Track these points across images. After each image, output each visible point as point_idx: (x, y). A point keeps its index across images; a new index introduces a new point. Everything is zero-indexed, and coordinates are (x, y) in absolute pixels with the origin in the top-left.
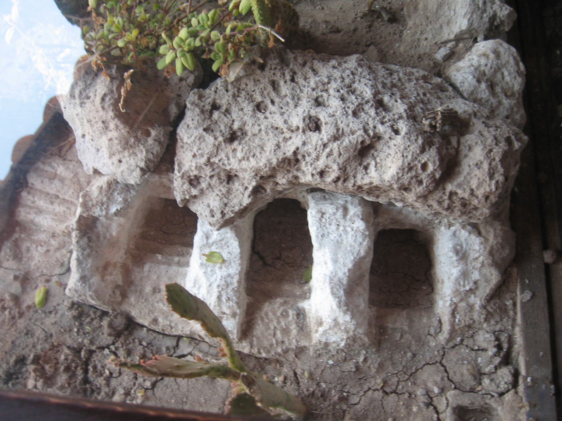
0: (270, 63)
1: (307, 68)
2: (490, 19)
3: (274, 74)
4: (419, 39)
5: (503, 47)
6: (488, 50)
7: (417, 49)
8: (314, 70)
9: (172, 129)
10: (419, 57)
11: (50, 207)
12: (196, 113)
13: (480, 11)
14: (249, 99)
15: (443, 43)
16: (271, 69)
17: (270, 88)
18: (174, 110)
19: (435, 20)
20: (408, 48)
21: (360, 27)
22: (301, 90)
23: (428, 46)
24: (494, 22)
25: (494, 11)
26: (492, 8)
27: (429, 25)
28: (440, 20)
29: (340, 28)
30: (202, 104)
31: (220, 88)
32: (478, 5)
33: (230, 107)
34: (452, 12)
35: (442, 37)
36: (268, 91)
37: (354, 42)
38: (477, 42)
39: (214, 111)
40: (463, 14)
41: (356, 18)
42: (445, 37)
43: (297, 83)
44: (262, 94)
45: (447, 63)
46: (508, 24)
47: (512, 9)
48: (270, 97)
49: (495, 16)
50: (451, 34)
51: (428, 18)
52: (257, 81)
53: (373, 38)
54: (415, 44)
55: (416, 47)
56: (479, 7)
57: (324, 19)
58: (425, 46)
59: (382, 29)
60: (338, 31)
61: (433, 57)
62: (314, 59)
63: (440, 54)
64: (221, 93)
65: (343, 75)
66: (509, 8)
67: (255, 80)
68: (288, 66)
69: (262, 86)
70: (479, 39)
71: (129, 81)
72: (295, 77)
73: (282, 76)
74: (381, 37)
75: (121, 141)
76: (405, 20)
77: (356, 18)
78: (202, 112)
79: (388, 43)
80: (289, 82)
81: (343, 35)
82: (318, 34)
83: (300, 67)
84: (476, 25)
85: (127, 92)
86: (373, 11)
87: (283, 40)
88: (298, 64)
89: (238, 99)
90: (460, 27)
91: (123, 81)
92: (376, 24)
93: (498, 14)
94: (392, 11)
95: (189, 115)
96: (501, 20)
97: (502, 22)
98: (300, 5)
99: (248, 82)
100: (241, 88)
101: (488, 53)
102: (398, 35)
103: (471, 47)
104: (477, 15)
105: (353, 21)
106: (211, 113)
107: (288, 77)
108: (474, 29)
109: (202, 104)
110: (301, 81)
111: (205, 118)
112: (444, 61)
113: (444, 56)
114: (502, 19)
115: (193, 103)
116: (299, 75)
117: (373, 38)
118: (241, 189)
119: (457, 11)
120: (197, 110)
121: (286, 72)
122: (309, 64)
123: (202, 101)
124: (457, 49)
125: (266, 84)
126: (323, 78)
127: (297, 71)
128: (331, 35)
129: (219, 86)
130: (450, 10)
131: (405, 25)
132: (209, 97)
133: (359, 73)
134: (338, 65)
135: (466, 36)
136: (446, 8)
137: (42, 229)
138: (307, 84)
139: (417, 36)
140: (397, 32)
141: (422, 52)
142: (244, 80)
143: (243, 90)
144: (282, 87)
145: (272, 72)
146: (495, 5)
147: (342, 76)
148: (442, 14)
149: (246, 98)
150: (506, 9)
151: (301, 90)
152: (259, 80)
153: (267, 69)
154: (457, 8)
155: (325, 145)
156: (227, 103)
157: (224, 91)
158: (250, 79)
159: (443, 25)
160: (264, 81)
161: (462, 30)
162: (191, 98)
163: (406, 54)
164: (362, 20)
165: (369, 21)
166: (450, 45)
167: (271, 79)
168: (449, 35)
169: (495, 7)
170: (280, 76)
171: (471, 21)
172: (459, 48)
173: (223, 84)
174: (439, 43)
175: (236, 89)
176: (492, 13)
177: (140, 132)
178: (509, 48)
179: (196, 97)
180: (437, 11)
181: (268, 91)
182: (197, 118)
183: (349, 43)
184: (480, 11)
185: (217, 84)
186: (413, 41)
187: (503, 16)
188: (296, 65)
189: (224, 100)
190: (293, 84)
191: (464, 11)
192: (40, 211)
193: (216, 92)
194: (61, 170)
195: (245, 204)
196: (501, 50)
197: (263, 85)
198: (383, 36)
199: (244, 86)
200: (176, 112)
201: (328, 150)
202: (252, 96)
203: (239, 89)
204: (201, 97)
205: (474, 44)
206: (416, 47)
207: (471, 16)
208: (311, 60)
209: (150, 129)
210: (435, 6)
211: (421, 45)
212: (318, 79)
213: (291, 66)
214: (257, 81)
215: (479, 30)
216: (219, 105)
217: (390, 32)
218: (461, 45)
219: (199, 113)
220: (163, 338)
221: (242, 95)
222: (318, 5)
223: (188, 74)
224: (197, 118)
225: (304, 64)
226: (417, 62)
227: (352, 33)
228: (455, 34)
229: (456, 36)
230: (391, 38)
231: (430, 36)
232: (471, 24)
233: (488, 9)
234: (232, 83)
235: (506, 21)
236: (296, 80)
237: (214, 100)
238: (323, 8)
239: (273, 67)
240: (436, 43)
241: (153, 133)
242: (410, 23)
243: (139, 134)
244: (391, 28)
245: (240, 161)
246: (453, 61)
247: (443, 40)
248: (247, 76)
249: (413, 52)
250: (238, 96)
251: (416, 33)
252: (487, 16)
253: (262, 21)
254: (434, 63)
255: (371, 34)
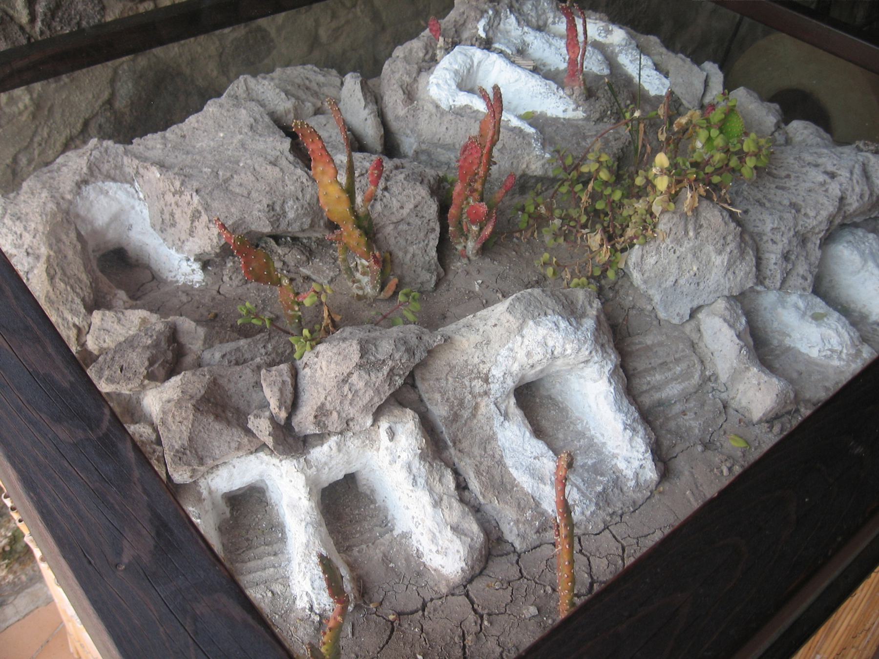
11: (669, 375)
75: (634, 430)
118: (813, 246)
137: (673, 402)
155: (851, 179)
192: (658, 388)
194: (649, 340)
195: (819, 257)
201: (855, 181)
220: (495, 163)
245: (815, 217)
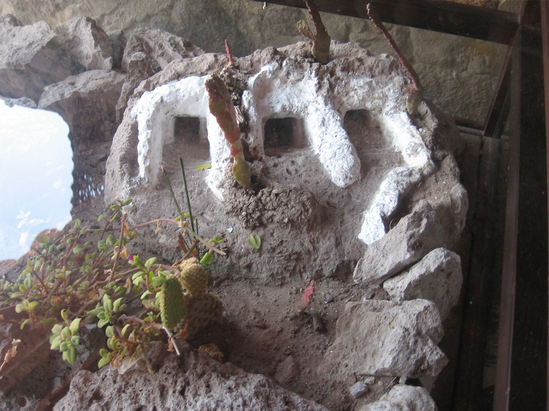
0: (167, 365)
1: (202, 382)
2: (417, 361)
3: (166, 379)
4: (339, 364)
5: (422, 400)
6: (404, 401)
7: (334, 375)
8: (208, 386)
9: (49, 403)
10: (333, 386)
12: (74, 399)
14: (132, 399)
15: (362, 375)
16: (165, 372)
17: (157, 393)
18: (58, 384)
19: (361, 346)
20: (325, 371)
21: (286, 329)
22: (185, 407)
23: (346, 374)
24: (421, 365)
25: (424, 354)
26: (422, 349)
27: (354, 351)
28: (367, 347)
29: (267, 324)
30: (85, 389)
31: (108, 377)
32: (409, 343)
34: (381, 344)
35: (363, 369)
36: (154, 395)
37: (275, 346)
38: (398, 383)
39: (94, 401)
40: (390, 350)
41: (286, 317)
42: (366, 371)
43: (185, 397)
45: (359, 400)
46: (436, 370)
47: (443, 355)
48: (154, 404)
49: (424, 358)
50: (373, 368)
51: (355, 342)
52: (147, 381)
53: (296, 346)
54: (334, 368)
55: (333, 372)
56: (408, 346)
57: (255, 307)
58: (343, 374)
59: (308, 338)
60: (264, 327)
61: (346, 390)
62: (214, 371)
63: (356, 389)
64: (108, 382)
65: (234, 403)
66: (441, 353)
67: (145, 379)
68: (185, 372)
69: (150, 388)
70: (400, 381)
71: (15, 347)
72: (187, 389)
73: (173, 383)
74: (304, 347)
76: (334, 334)
77: (286, 317)
78: (82, 399)
79: (308, 358)
80: (177, 394)
81: (266, 334)
84: (400, 365)
86: (306, 314)
87: (178, 354)
88: (195, 374)
89: (123, 395)
90: (383, 364)
91: (10, 346)
92: (304, 329)
93: (427, 358)
94: (325, 318)
95: (68, 396)
96: (428, 365)
97: (429, 367)
98: (239, 283)
99: (138, 378)
100: (130, 382)
101: (402, 404)
102: (321, 351)
103: (390, 388)
104: (404, 355)
105: (282, 321)
106: (90, 402)
107: (179, 388)
108: (397, 369)
109: (85, 389)
110: (189, 395)
111: (81, 407)
112: (357, 398)
114: (430, 364)
115: (76, 386)
116: (191, 388)
117: (296, 346)
119: (385, 343)
120: (77, 396)
121: (179, 380)
123: (86, 386)
124: (374, 387)
125: (155, 387)
126: (212, 402)
127: (191, 382)
128: (255, 328)
129: (108, 374)
130: (379, 340)
131: (332, 340)
132: (95, 384)
133: (251, 405)
134: (235, 387)
135: (388, 374)
136: (376, 336)
138: (194, 403)
139: (339, 359)
140: (321, 347)
141: (338, 380)
142: (135, 376)
143: (131, 386)
144: (169, 397)
145: (165, 376)
146: (426, 347)
148: (370, 341)
149: (130, 396)
150: (437, 353)
151: (185, 407)
152: (149, 380)
153: (161, 371)
154: (386, 341)
156: (110, 396)
157: (112, 382)
158: (141, 377)
159: (368, 355)
160: (154, 383)
161: (384, 368)
162: (77, 379)
164: (291, 322)
166: (368, 380)
167: (162, 383)
168: (370, 368)
169: (426, 349)
170: (172, 384)
171: (396, 360)
172: (377, 385)
173: (112, 374)
174: (358, 374)
175: (124, 383)
176: (420, 356)
177: (15, 400)
178: (428, 402)
179: (81, 380)
180: (366, 337)
181: (154, 395)
183: (269, 346)
184: (409, 350)
187: (432, 361)
188: (193, 374)
189: (108, 393)
190: (181, 398)
191: (391, 347)
193: (103, 380)
196: (419, 403)
197: (152, 387)
198: (306, 346)
199: (134, 382)
200: (60, 386)
202: (137, 395)
203: (128, 383)
204: (86, 380)
205: (394, 385)
206: (333, 372)
207: (398, 355)
208: (210, 371)
209: (26, 398)
210: (366, 331)
211: (340, 371)
212: (206, 401)
213: (187, 374)
214: (147, 381)
216: (102, 395)
217: (314, 345)
218: (380, 383)
221: (128, 391)
222: (255, 290)
223: (84, 349)
224: (73, 405)
225: (201, 376)
226: (329, 390)
227: (276, 334)
228: (377, 369)
229: (377, 372)
230: (312, 352)
231: (352, 364)
232: (395, 363)
233: (418, 349)
234: (122, 376)
236: (186, 394)
237: (99, 388)
239: (168, 370)
240: (355, 374)
241: (28, 404)
242: (338, 341)
243: (13, 402)
244: (318, 339)
246: (366, 400)
247: (362, 373)
248: (140, 372)
250: (124, 392)
251: (339, 356)
252: (415, 358)
253: (166, 323)
254: (346, 398)
255: (295, 341)
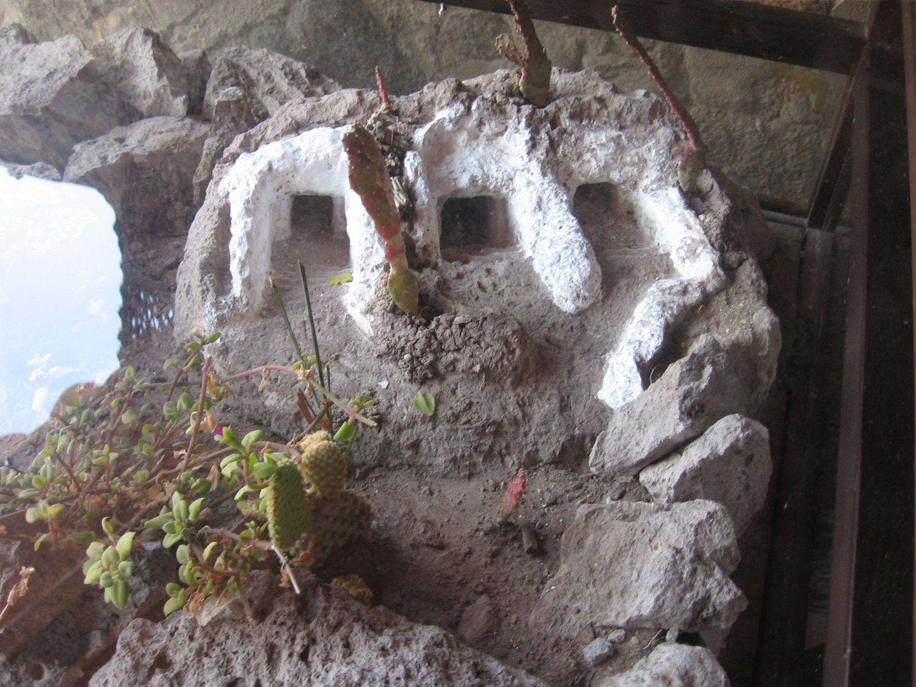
0: (278, 610)
1: (337, 638)
2: (696, 604)
3: (277, 633)
4: (566, 608)
5: (704, 669)
6: (674, 671)
7: (557, 626)
8: (347, 645)
9: (82, 674)
10: (556, 644)
13: (682, 586)
14: (221, 667)
15: (604, 627)
16: (275, 622)
17: (262, 658)
18: (97, 642)
19: (603, 579)
20: (542, 620)
21: (478, 549)
22: (309, 681)
23: (578, 625)
24: (702, 610)
25: (707, 591)
26: (704, 584)
27: (591, 586)
28: (612, 580)
29: (446, 541)
30: (142, 650)
31: (181, 630)
32: (682, 573)
33: (186, 671)
35: (606, 616)
36: (258, 660)
37: (459, 578)
38: (664, 640)
39: (157, 670)
40: (651, 585)
41: (477, 530)
43: (308, 664)
44: (245, 666)
45: (599, 669)
46: (728, 619)
47: (740, 593)
48: (257, 675)
49: (707, 598)
50: (622, 614)
51: (592, 571)
52: (245, 637)
53: (493, 578)
54: (558, 616)
55: (556, 622)
56: (681, 579)
57: (425, 514)
58: (572, 625)
59: (513, 564)
60: (441, 547)
61: (578, 652)
62: (357, 620)
63: (593, 650)
64: (180, 639)
65: (390, 674)
66: (735, 589)
67: (242, 634)
68: (308, 621)
69: (251, 648)
70: (668, 637)
71: (26, 581)
72: (311, 650)
73: (289, 640)
74: (507, 580)
76: (558, 558)
77: (477, 530)
78: (136, 667)
79: (514, 598)
80: (295, 658)
81: (444, 558)
82: (405, 542)
83: (326, 633)
84: (667, 611)
85: (17, 599)
86: (510, 524)
87: (298, 591)
88: (325, 624)
89: (205, 660)
90: (639, 608)
91: (17, 578)
92: (507, 549)
93: (713, 598)
94: (543, 532)
95: (114, 662)
96: (715, 610)
97: (717, 614)
99: (231, 632)
100: (217, 639)
101: (671, 676)
102: (535, 587)
103: (651, 649)
104: (674, 593)
106: (151, 673)
107: (298, 648)
109: (142, 650)
110: (316, 661)
111: (136, 681)
112: (595, 665)
113: (597, 657)
114: (718, 608)
115: (126, 646)
116: (319, 648)
117: (493, 578)
119: (642, 574)
120: (129, 661)
121: (299, 635)
122: (343, 630)
123: (143, 645)
124: (625, 647)
126: (354, 672)
127: (319, 639)
128: (426, 549)
129: (180, 626)
130: (633, 568)
131: (553, 568)
132: (158, 641)
133: (419, 678)
134: (392, 647)
135: (648, 625)
136: (628, 562)
138: (323, 673)
139: (565, 601)
140: (536, 580)
142: (226, 628)
143: (218, 645)
144: (282, 664)
145: (275, 628)
146: (711, 580)
147: (387, 676)
148: (617, 570)
149: (217, 662)
150: (730, 590)
151: (309, 681)
152: (249, 636)
153: (269, 620)
154: (644, 570)
156: (183, 662)
157: (186, 638)
158: (235, 630)
159: (614, 593)
160: (257, 640)
162: (128, 634)
163: (536, 631)
164: (485, 538)
165: (496, 544)
167: (271, 640)
168: (618, 615)
169: (711, 583)
170: (286, 641)
171: (660, 602)
172: (628, 644)
173: (188, 625)
174: (598, 625)
175: (207, 640)
177: (25, 668)
178: (714, 672)
179: (136, 635)
180: (611, 562)
181: (258, 660)
182: (122, 676)
183: (449, 578)
184: (682, 586)
185: (180, 621)
186: (554, 609)
187: (721, 603)
188: (322, 624)
189: (180, 656)
190: (302, 665)
191: (653, 580)
193: (172, 634)
196: (698, 674)
197: (253, 648)
198: (511, 579)
199: (223, 639)
200: (100, 645)
202: (229, 661)
203: (213, 640)
204: (144, 636)
205: (657, 643)
206: (556, 622)
207: (664, 593)
208: (351, 620)
209: (44, 666)
210: (610, 553)
211: (567, 620)
212: (344, 670)
213: (312, 625)
214: (245, 637)
215: (672, 621)
216: (171, 661)
218: (634, 640)
219: (129, 667)
221: (214, 654)
222: (426, 484)
224: (122, 676)
225: (335, 629)
226: (549, 651)
227: (460, 558)
228: (628, 617)
229: (628, 621)
230: (521, 589)
231: (586, 608)
232: (659, 607)
233: (698, 584)
234: (203, 628)
235: (724, 614)
236: (310, 658)
237: (165, 648)
238: (431, 493)
239: (281, 619)
240: (592, 625)
241: (47, 675)
242: (563, 569)
243: (22, 671)
247: (604, 623)
248: (234, 621)
249: (549, 629)
250: (207, 655)
251: (565, 594)
252: (692, 598)
253: (277, 540)
254: (578, 665)
255: (493, 569)
